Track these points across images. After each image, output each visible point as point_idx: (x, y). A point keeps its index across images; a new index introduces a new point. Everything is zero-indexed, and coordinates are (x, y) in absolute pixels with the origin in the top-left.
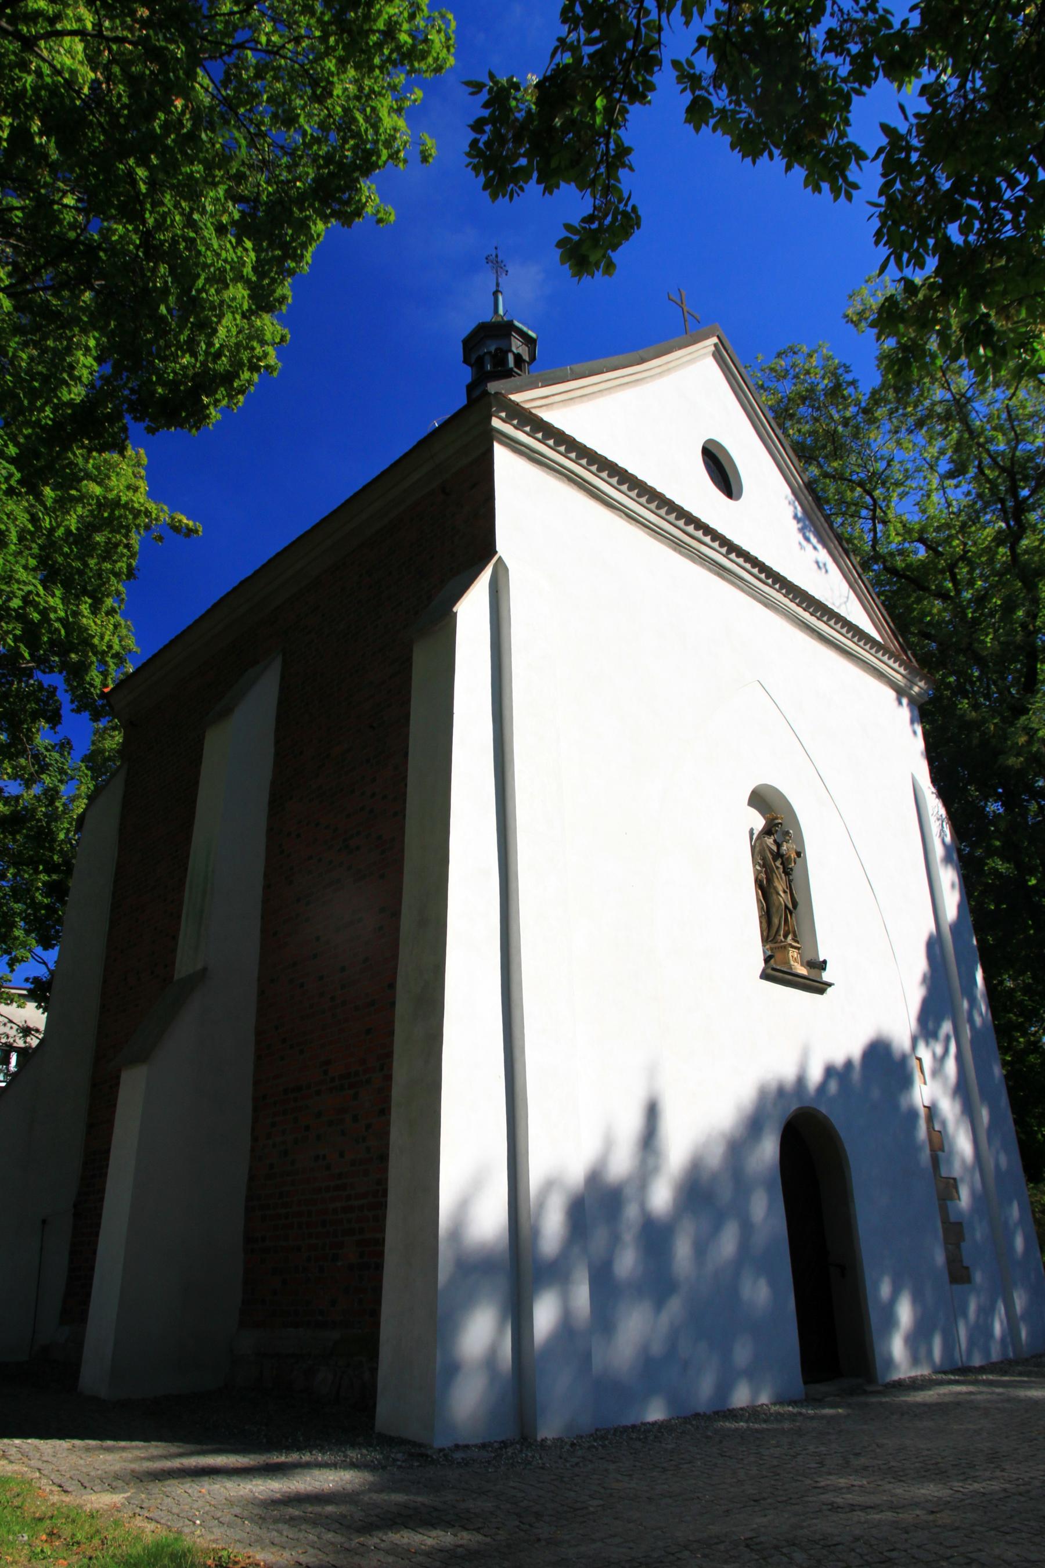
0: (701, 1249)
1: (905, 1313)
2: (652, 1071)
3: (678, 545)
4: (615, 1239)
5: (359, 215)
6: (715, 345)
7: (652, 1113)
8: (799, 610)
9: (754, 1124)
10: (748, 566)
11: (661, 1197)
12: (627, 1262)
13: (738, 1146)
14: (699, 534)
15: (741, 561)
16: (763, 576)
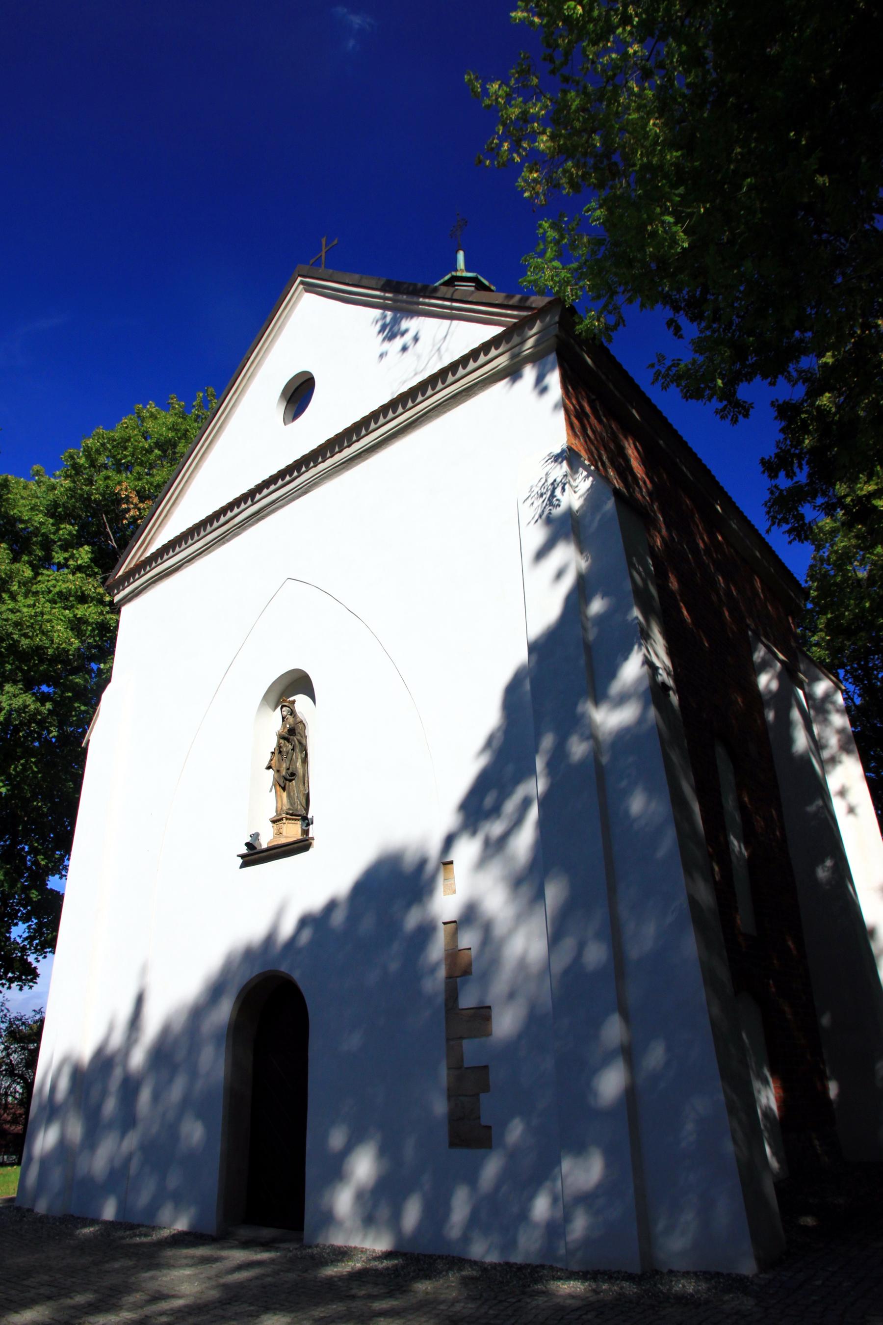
0: (156, 1097)
1: (363, 1167)
2: (144, 970)
3: (222, 540)
4: (104, 1093)
5: (486, 1088)
6: (302, 283)
7: (140, 1001)
8: (321, 467)
9: (215, 991)
10: (273, 487)
11: (138, 1058)
12: (110, 1106)
13: (197, 1013)
14: (230, 514)
15: (265, 492)
16: (288, 478)
